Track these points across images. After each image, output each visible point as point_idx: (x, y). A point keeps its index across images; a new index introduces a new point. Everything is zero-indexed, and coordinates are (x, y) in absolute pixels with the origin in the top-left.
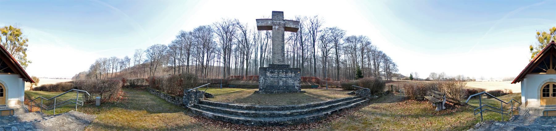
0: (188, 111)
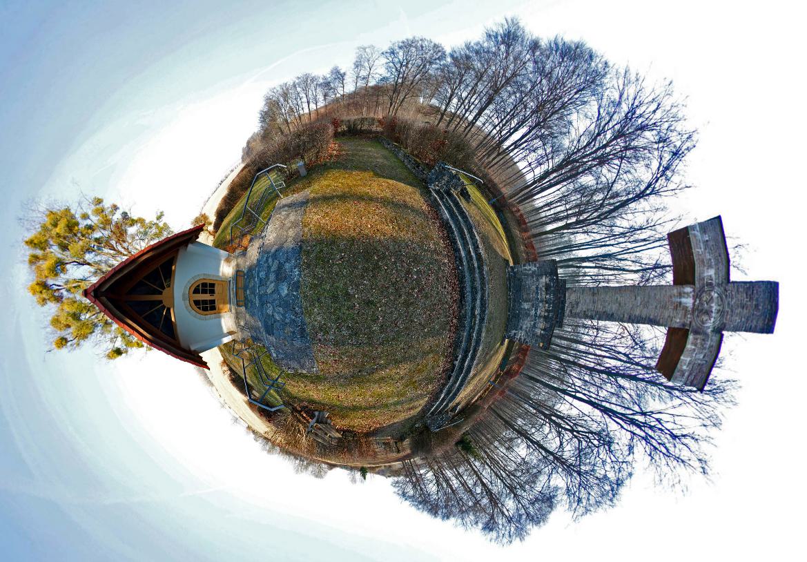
0: (426, 192)
